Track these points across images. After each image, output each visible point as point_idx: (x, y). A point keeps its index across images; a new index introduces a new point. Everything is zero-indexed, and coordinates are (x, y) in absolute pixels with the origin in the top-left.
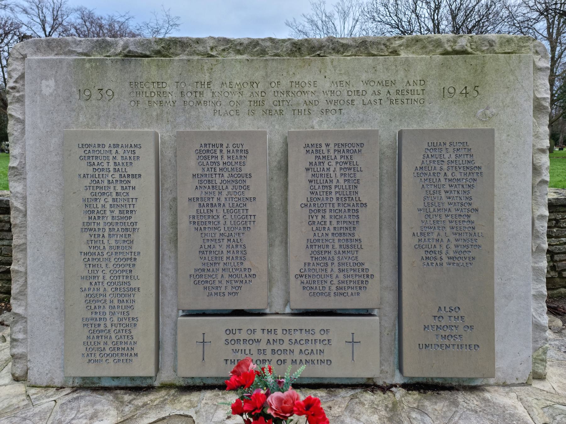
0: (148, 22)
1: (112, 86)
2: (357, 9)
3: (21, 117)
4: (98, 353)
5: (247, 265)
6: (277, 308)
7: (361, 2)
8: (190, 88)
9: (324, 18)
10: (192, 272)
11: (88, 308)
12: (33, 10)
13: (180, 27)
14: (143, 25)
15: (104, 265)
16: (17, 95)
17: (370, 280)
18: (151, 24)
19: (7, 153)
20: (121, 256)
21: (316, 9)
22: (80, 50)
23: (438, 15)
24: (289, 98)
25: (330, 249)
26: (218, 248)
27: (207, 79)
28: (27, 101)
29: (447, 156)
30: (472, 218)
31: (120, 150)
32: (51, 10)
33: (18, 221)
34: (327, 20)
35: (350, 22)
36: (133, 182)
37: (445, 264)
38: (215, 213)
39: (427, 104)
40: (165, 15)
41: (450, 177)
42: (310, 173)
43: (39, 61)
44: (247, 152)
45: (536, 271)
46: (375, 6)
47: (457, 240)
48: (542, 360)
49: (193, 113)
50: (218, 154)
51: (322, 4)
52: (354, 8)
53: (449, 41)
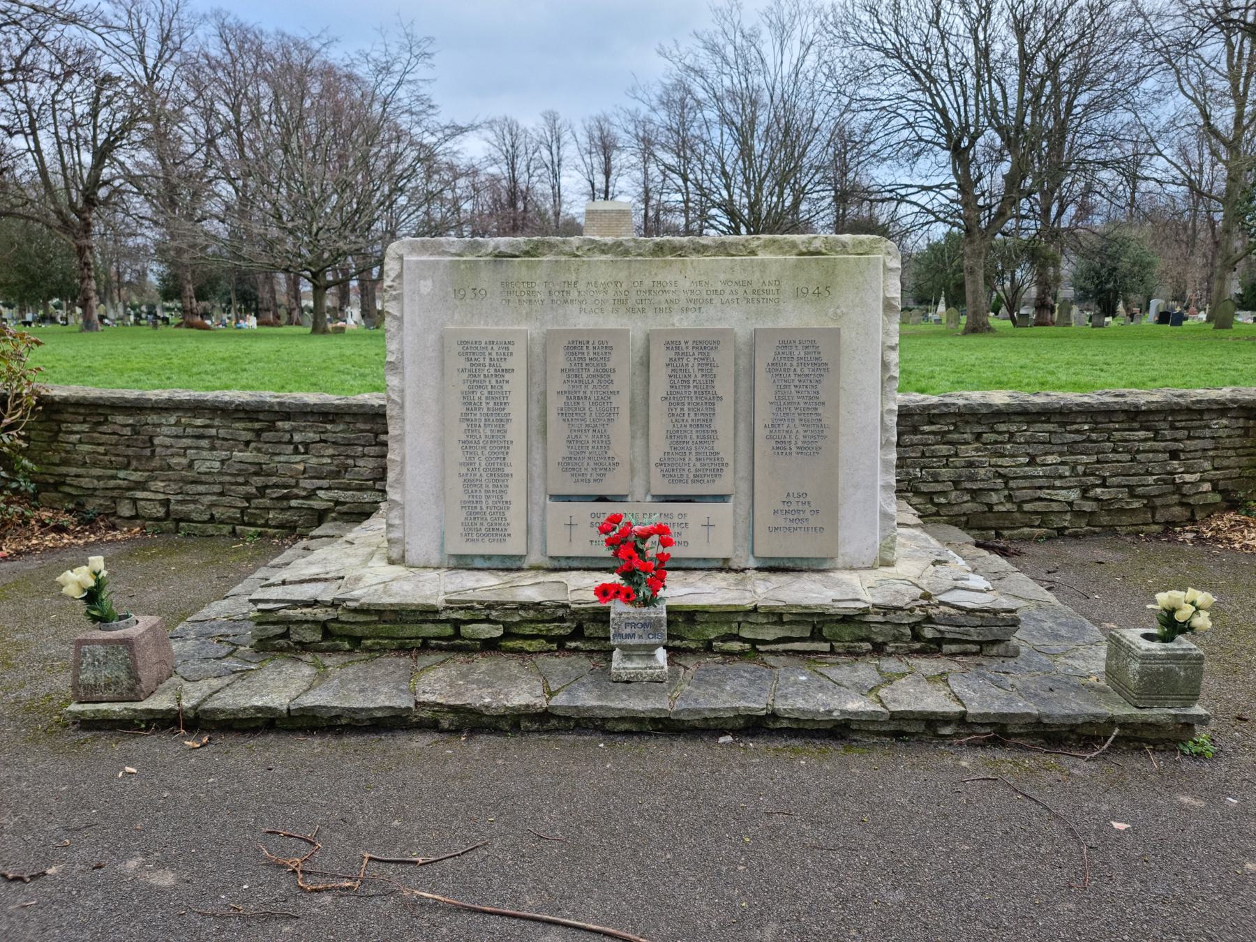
0: (367, 51)
1: (485, 286)
2: (810, 19)
3: (398, 314)
4: (475, 533)
5: (610, 454)
6: (638, 496)
7: (817, 5)
8: (557, 288)
9: (739, 40)
10: (560, 460)
11: (466, 492)
12: (120, 18)
13: (434, 60)
14: (358, 56)
15: (480, 452)
16: (394, 293)
17: (724, 468)
18: (375, 55)
19: (63, 325)
20: (496, 445)
21: (723, 20)
22: (453, 251)
23: (985, 29)
24: (650, 297)
25: (688, 439)
26: (584, 438)
27: (574, 279)
28: (406, 300)
29: (796, 353)
30: (819, 411)
31: (494, 347)
32: (157, 19)
33: (394, 413)
34: (744, 43)
35: (794, 49)
36: (507, 377)
37: (794, 454)
38: (581, 405)
39: (781, 303)
40: (403, 34)
41: (799, 372)
42: (670, 368)
43: (418, 262)
44: (611, 348)
45: (885, 463)
46: (851, 11)
47: (805, 431)
48: (891, 548)
49: (560, 311)
50: (585, 350)
51: (734, 9)
52: (804, 17)
53: (803, 242)
